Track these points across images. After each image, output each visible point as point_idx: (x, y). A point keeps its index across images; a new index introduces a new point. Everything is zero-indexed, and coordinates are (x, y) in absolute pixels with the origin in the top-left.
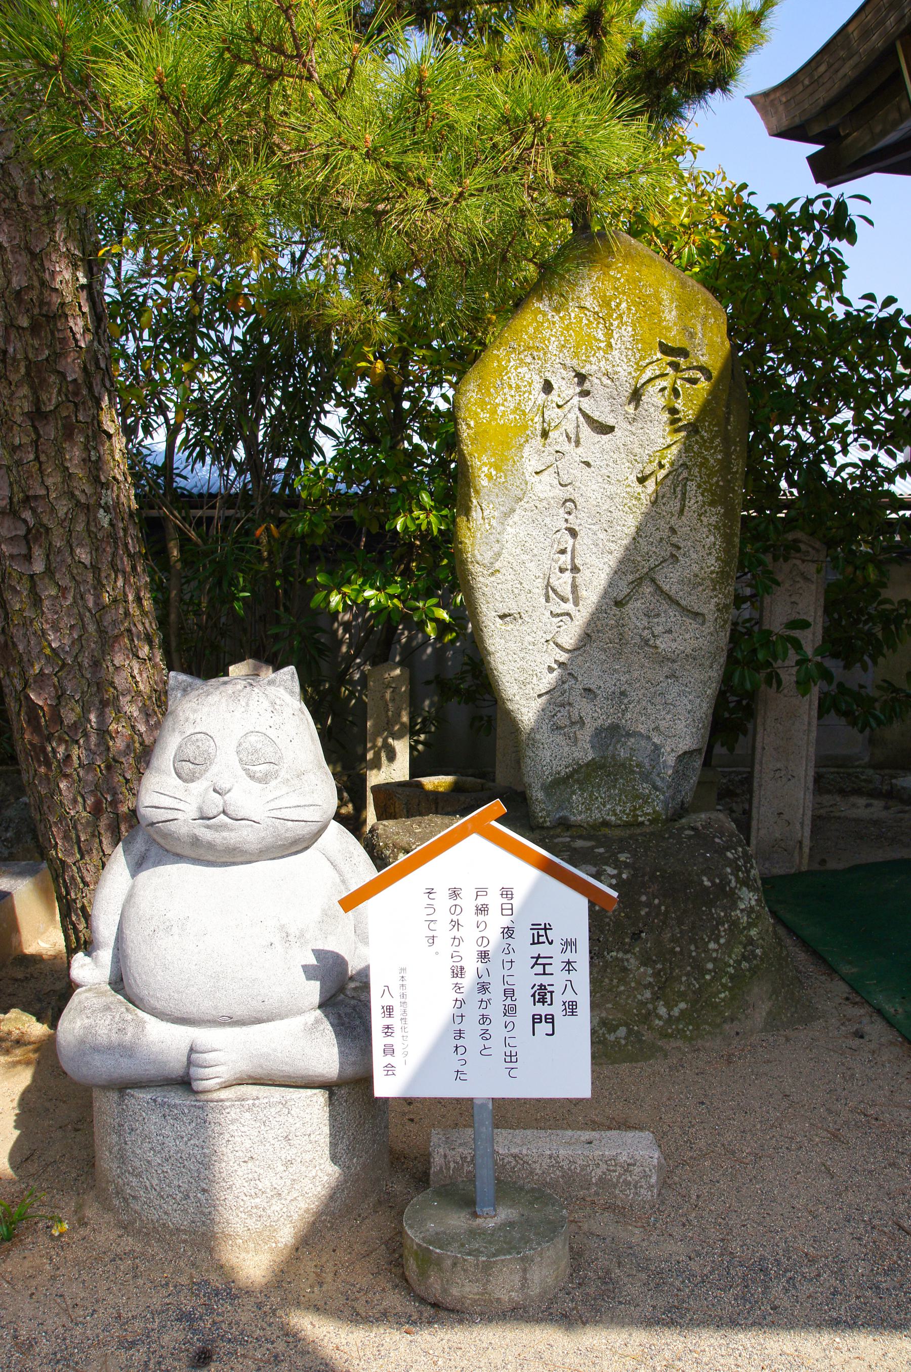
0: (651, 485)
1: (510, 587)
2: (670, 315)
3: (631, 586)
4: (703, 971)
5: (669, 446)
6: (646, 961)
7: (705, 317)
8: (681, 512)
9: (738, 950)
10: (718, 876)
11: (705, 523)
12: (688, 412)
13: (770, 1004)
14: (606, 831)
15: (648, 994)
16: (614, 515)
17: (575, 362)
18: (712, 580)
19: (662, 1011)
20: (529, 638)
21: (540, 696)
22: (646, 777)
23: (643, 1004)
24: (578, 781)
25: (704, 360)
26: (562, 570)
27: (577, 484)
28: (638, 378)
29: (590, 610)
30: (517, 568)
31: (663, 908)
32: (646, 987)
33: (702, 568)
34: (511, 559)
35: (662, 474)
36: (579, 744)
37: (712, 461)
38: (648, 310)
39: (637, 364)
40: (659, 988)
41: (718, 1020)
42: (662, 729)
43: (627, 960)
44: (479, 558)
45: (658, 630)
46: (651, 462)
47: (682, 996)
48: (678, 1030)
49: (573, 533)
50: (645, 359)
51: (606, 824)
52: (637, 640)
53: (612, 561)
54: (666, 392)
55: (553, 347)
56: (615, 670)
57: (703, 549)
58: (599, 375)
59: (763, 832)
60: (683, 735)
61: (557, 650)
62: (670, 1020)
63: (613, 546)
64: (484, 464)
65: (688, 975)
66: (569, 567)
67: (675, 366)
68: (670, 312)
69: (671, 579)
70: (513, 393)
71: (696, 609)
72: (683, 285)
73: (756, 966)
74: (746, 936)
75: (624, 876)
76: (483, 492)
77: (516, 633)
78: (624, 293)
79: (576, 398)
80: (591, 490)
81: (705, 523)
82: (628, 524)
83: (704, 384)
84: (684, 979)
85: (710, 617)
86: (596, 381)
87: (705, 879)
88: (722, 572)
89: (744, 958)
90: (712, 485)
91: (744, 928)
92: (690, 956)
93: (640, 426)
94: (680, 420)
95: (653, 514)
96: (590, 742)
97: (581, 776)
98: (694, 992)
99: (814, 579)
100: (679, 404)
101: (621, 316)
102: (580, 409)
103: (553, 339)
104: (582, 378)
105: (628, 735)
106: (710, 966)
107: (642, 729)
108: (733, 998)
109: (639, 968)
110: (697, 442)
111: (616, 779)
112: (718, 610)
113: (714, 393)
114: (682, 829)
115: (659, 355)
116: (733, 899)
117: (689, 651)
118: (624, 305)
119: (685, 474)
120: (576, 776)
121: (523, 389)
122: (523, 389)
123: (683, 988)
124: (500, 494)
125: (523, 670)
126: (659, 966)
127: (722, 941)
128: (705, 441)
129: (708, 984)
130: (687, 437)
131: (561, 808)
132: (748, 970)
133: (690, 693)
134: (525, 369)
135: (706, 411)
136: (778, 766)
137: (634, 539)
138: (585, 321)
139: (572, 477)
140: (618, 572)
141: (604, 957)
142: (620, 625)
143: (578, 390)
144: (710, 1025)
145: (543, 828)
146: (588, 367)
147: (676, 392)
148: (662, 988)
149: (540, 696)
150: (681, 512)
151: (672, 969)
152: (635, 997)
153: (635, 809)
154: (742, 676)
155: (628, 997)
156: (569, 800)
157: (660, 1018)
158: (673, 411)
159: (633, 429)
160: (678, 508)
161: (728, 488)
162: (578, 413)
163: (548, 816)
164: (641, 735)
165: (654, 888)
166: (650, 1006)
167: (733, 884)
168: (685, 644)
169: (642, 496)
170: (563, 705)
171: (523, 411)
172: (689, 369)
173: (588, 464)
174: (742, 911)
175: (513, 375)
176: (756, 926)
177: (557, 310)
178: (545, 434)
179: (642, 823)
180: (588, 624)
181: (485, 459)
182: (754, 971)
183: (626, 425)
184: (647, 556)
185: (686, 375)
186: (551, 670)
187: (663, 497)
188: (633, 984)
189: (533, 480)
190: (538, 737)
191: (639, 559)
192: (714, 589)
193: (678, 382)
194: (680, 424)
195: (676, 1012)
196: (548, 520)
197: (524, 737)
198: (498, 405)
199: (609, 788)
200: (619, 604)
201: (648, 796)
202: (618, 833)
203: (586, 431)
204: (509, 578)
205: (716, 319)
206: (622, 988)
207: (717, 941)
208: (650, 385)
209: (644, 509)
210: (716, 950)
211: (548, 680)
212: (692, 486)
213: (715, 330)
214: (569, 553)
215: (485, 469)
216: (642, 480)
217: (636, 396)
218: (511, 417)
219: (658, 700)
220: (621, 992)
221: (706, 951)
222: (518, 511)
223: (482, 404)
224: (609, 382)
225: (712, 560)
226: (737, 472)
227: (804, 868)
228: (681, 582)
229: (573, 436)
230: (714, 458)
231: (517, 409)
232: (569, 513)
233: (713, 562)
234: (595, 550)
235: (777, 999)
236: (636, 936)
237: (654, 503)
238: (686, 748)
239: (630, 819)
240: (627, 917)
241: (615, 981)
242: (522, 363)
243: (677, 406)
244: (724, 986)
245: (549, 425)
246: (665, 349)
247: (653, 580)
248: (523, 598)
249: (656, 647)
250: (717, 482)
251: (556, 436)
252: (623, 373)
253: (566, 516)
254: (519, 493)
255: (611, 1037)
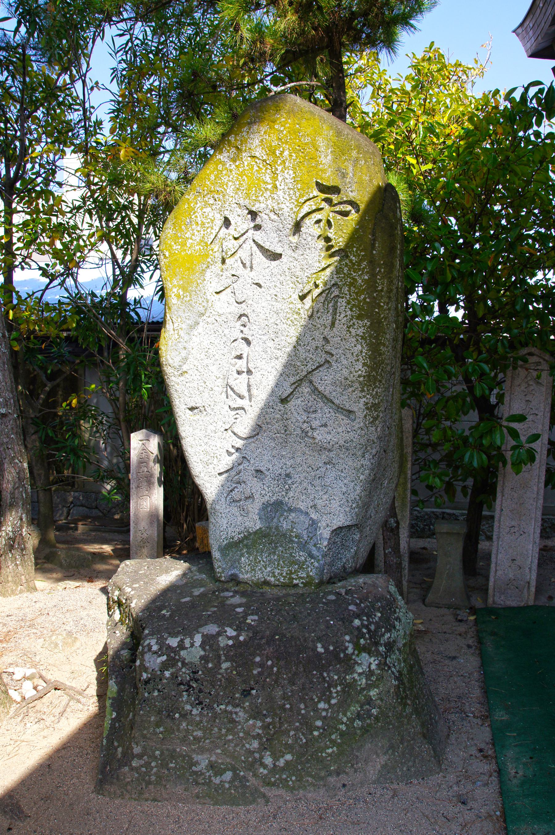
0: (308, 302)
1: (196, 386)
2: (326, 159)
3: (293, 387)
4: (312, 728)
5: (324, 269)
6: (255, 714)
7: (357, 160)
8: (333, 324)
9: (355, 708)
10: (333, 644)
11: (353, 333)
12: (339, 240)
13: (386, 757)
14: (267, 589)
15: (255, 744)
16: (279, 327)
17: (247, 202)
18: (360, 383)
19: (268, 760)
20: (212, 428)
21: (220, 474)
22: (303, 546)
23: (250, 752)
24: (246, 546)
25: (352, 196)
26: (239, 373)
27: (250, 302)
28: (297, 213)
29: (260, 406)
30: (202, 370)
31: (275, 669)
32: (254, 737)
33: (351, 372)
34: (196, 363)
35: (317, 292)
36: (250, 516)
37: (360, 281)
38: (307, 156)
39: (297, 201)
40: (267, 740)
41: (323, 774)
42: (319, 507)
43: (236, 713)
44: (171, 361)
45: (315, 424)
46: (309, 282)
47: (290, 748)
48: (280, 779)
49: (248, 342)
50: (303, 196)
51: (266, 583)
52: (299, 431)
53: (279, 365)
54: (322, 224)
55: (230, 191)
56: (282, 456)
57: (350, 356)
58: (267, 211)
59: (499, 573)
60: (337, 512)
61: (234, 437)
62: (275, 769)
63: (279, 353)
64: (175, 286)
65: (296, 729)
66: (245, 370)
67: (328, 201)
68: (326, 156)
69: (325, 381)
70: (199, 228)
71: (347, 407)
72: (339, 133)
73: (369, 725)
74: (365, 696)
75: (241, 638)
76: (174, 308)
77: (201, 423)
78: (286, 143)
79: (251, 232)
80: (261, 306)
81: (353, 333)
82: (291, 334)
83: (354, 216)
84: (292, 733)
85: (360, 414)
86: (266, 217)
87: (319, 645)
88: (369, 376)
89: (359, 716)
90: (360, 302)
91: (363, 689)
92: (299, 714)
93: (301, 253)
94: (332, 246)
95: (310, 326)
96: (258, 514)
97: (250, 542)
98: (301, 746)
99: (545, 384)
100: (331, 234)
101: (284, 162)
102: (254, 241)
103: (230, 183)
104: (253, 214)
105: (290, 510)
106: (319, 723)
107: (302, 506)
108: (341, 753)
109: (247, 721)
110: (346, 265)
111: (276, 547)
112: (367, 408)
113: (361, 223)
114: (327, 594)
115: (316, 192)
116: (348, 664)
117: (341, 442)
118: (286, 153)
119: (336, 293)
120: (245, 542)
121: (207, 225)
122: (207, 225)
123: (290, 741)
124: (186, 310)
125: (206, 453)
126: (269, 720)
127: (333, 701)
128: (354, 264)
129: (316, 739)
130: (340, 261)
131: (232, 567)
132: (360, 729)
133: (345, 478)
134: (209, 209)
135: (355, 238)
136: (513, 523)
137: (295, 347)
138: (256, 168)
139: (245, 296)
140: (283, 375)
141: (213, 708)
142: (284, 419)
143: (252, 225)
144: (313, 777)
145: (220, 581)
146: (257, 205)
147: (329, 223)
148: (269, 742)
149: (220, 474)
150: (333, 324)
151: (281, 724)
152: (244, 745)
153: (291, 573)
154: (472, 456)
155: (237, 745)
156: (239, 561)
157: (265, 766)
158: (328, 239)
159: (296, 256)
160: (329, 321)
161: (374, 303)
162: (252, 243)
163: (223, 572)
164: (301, 511)
165: (269, 650)
166: (257, 755)
167: (350, 650)
168: (337, 436)
169: (302, 311)
170: (239, 483)
171: (206, 243)
172: (340, 203)
173: (259, 286)
174: (360, 674)
175: (199, 213)
176: (377, 687)
177: (234, 160)
178: (223, 261)
179: (296, 585)
180: (259, 417)
181: (175, 283)
182: (365, 730)
183: (290, 252)
184: (305, 362)
185: (337, 208)
186: (229, 453)
187: (318, 312)
188: (241, 735)
189: (213, 298)
190: (218, 507)
191: (299, 364)
192: (362, 391)
193: (331, 214)
194: (333, 250)
195: (281, 763)
196: (227, 332)
197: (209, 507)
198: (188, 238)
199: (270, 554)
200: (284, 401)
201: (304, 563)
202: (275, 591)
203: (259, 257)
204: (195, 378)
205: (366, 161)
206: (231, 737)
207: (328, 701)
208: (307, 218)
209: (303, 323)
210: (326, 710)
211: (227, 462)
212: (342, 303)
213: (365, 171)
214: (245, 358)
215: (175, 290)
216: (302, 298)
217: (297, 227)
218: (197, 248)
219: (317, 482)
220: (229, 740)
221: (316, 710)
222: (201, 324)
223: (176, 238)
224: (276, 217)
225: (359, 366)
226: (382, 290)
227: (531, 603)
228: (334, 384)
229: (248, 265)
230: (362, 279)
231: (201, 241)
232: (244, 326)
233: (360, 367)
234: (265, 356)
235: (393, 754)
236: (246, 693)
237: (311, 317)
238: (340, 524)
239: (287, 581)
240: (239, 674)
241: (224, 731)
242: (207, 204)
243: (330, 235)
244: (333, 742)
245: (226, 254)
246: (322, 188)
247: (311, 382)
248: (206, 395)
249: (314, 438)
250: (365, 299)
251: (232, 263)
252: (286, 210)
253: (242, 328)
254: (202, 309)
255: (217, 780)
